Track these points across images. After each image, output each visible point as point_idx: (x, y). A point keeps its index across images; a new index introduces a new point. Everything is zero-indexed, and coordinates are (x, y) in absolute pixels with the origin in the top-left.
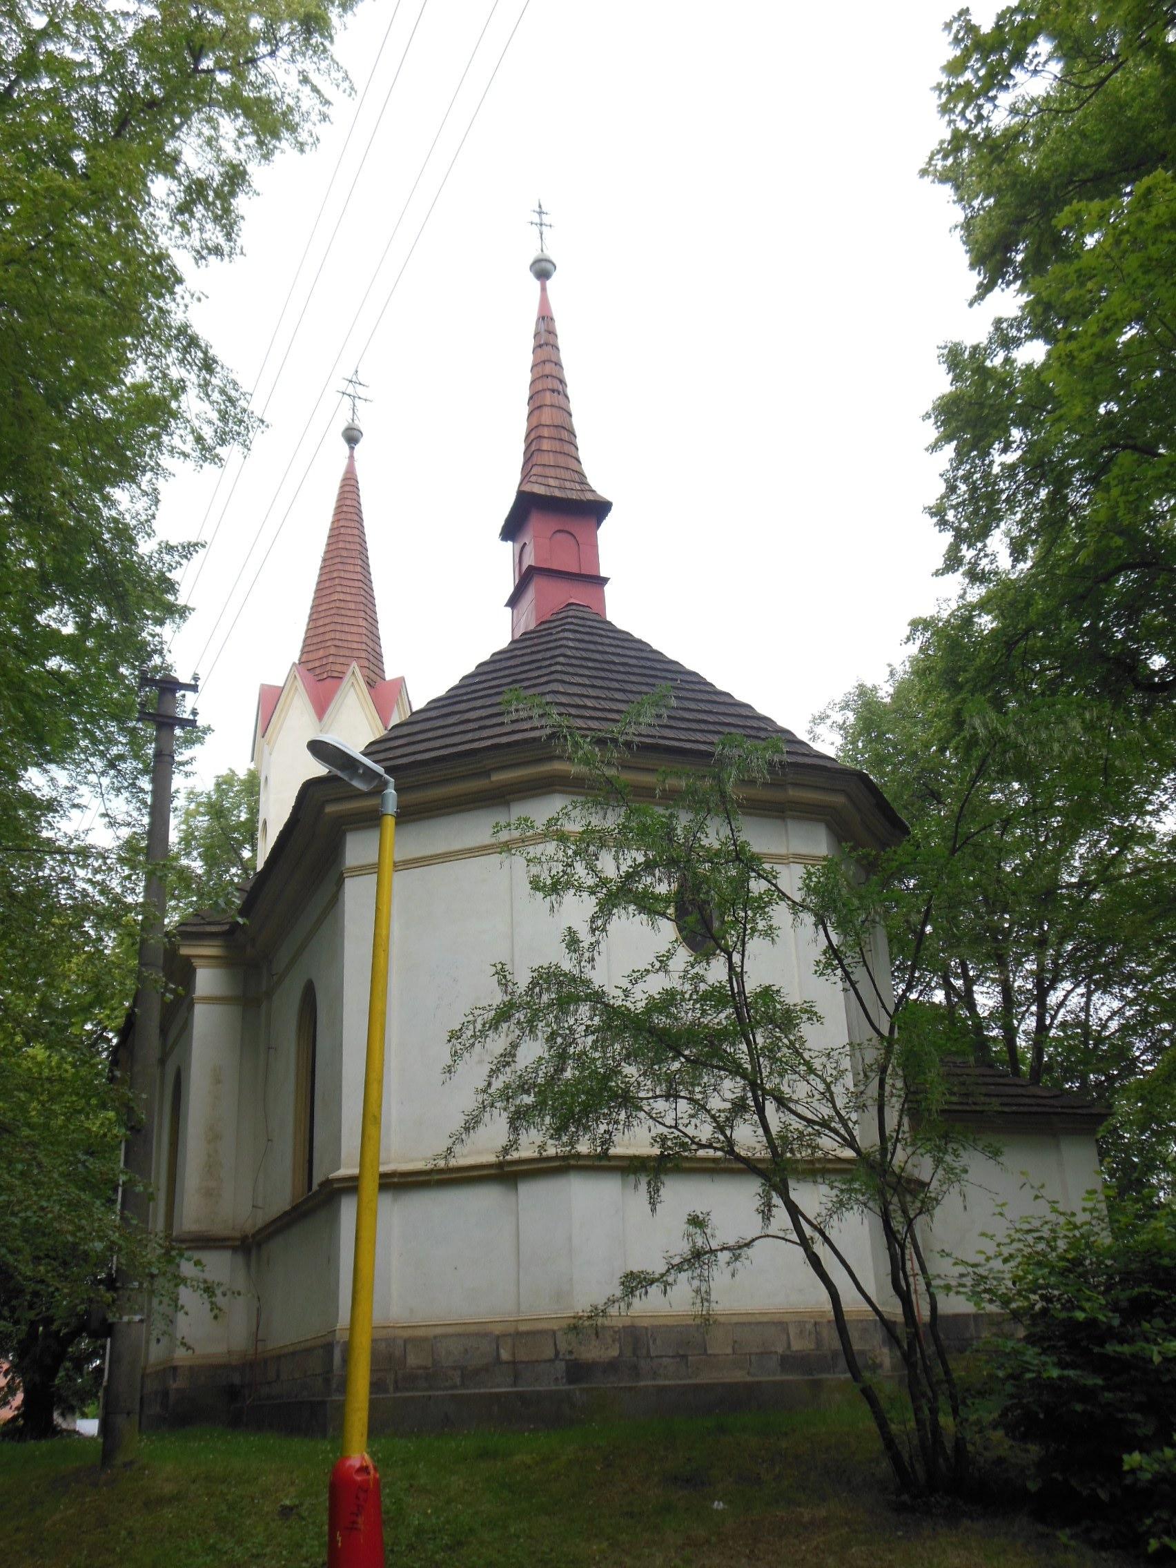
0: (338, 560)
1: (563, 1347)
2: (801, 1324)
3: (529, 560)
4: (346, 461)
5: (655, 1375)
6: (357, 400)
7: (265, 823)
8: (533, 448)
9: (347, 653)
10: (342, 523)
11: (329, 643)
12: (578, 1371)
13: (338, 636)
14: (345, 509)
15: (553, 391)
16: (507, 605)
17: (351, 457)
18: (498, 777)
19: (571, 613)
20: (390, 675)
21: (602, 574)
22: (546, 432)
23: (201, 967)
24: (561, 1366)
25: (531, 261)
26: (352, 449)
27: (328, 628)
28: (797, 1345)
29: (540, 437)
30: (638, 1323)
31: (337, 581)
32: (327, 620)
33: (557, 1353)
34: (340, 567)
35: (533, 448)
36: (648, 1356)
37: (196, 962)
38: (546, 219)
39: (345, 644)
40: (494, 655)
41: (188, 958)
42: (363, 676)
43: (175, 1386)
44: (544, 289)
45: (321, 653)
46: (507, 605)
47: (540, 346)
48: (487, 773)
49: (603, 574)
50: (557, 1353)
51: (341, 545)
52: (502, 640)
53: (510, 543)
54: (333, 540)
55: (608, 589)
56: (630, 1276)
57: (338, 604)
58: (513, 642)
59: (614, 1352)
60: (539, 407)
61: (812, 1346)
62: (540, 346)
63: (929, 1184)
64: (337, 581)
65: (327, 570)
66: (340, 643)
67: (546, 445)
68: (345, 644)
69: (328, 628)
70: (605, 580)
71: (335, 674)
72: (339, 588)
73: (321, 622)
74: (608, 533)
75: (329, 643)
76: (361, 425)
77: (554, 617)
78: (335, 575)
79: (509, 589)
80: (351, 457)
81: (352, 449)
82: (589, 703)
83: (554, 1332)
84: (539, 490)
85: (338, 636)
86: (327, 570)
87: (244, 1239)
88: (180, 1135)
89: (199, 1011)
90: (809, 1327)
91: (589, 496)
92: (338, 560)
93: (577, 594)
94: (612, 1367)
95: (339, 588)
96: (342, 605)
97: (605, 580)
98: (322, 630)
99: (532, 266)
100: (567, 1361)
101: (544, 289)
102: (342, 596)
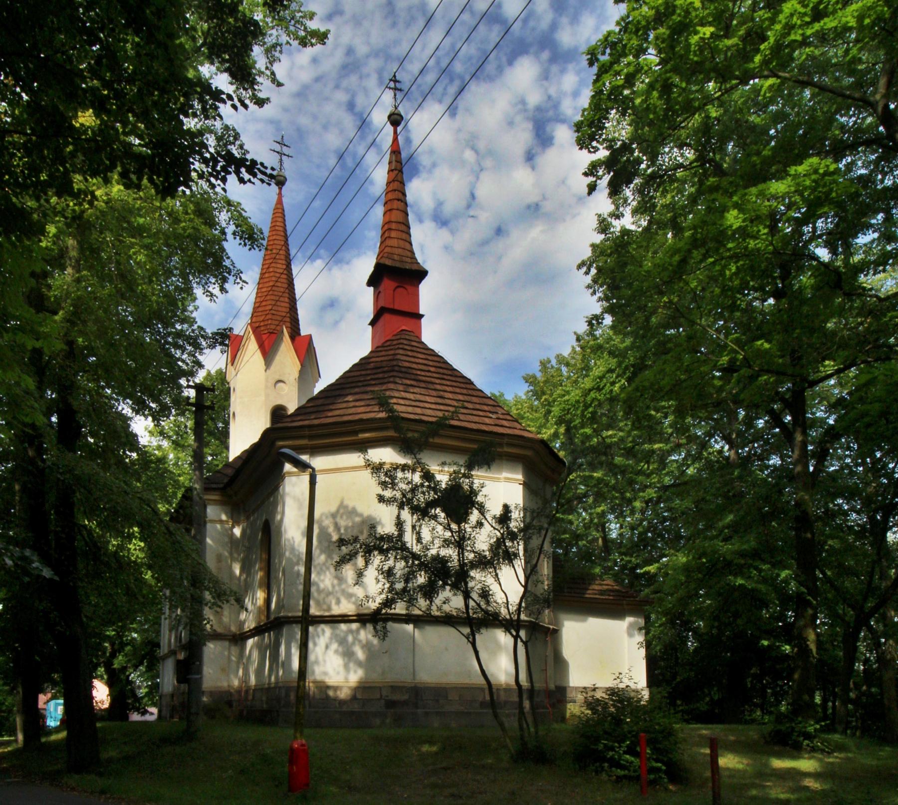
3: (382, 304)
4: (276, 197)
6: (284, 158)
7: (234, 414)
8: (386, 235)
15: (398, 200)
16: (370, 324)
17: (280, 194)
19: (403, 337)
22: (394, 226)
24: (383, 701)
25: (388, 114)
26: (280, 189)
30: (419, 685)
33: (381, 696)
35: (386, 235)
40: (361, 360)
46: (370, 324)
47: (392, 170)
48: (356, 433)
49: (421, 312)
52: (365, 349)
53: (372, 288)
55: (423, 320)
56: (380, 502)
58: (371, 352)
59: (405, 697)
60: (390, 210)
67: (393, 234)
70: (422, 316)
77: (394, 338)
79: (372, 317)
80: (280, 194)
81: (280, 189)
82: (432, 369)
84: (388, 262)
88: (438, 451)
91: (415, 267)
93: (405, 324)
94: (405, 703)
97: (422, 316)
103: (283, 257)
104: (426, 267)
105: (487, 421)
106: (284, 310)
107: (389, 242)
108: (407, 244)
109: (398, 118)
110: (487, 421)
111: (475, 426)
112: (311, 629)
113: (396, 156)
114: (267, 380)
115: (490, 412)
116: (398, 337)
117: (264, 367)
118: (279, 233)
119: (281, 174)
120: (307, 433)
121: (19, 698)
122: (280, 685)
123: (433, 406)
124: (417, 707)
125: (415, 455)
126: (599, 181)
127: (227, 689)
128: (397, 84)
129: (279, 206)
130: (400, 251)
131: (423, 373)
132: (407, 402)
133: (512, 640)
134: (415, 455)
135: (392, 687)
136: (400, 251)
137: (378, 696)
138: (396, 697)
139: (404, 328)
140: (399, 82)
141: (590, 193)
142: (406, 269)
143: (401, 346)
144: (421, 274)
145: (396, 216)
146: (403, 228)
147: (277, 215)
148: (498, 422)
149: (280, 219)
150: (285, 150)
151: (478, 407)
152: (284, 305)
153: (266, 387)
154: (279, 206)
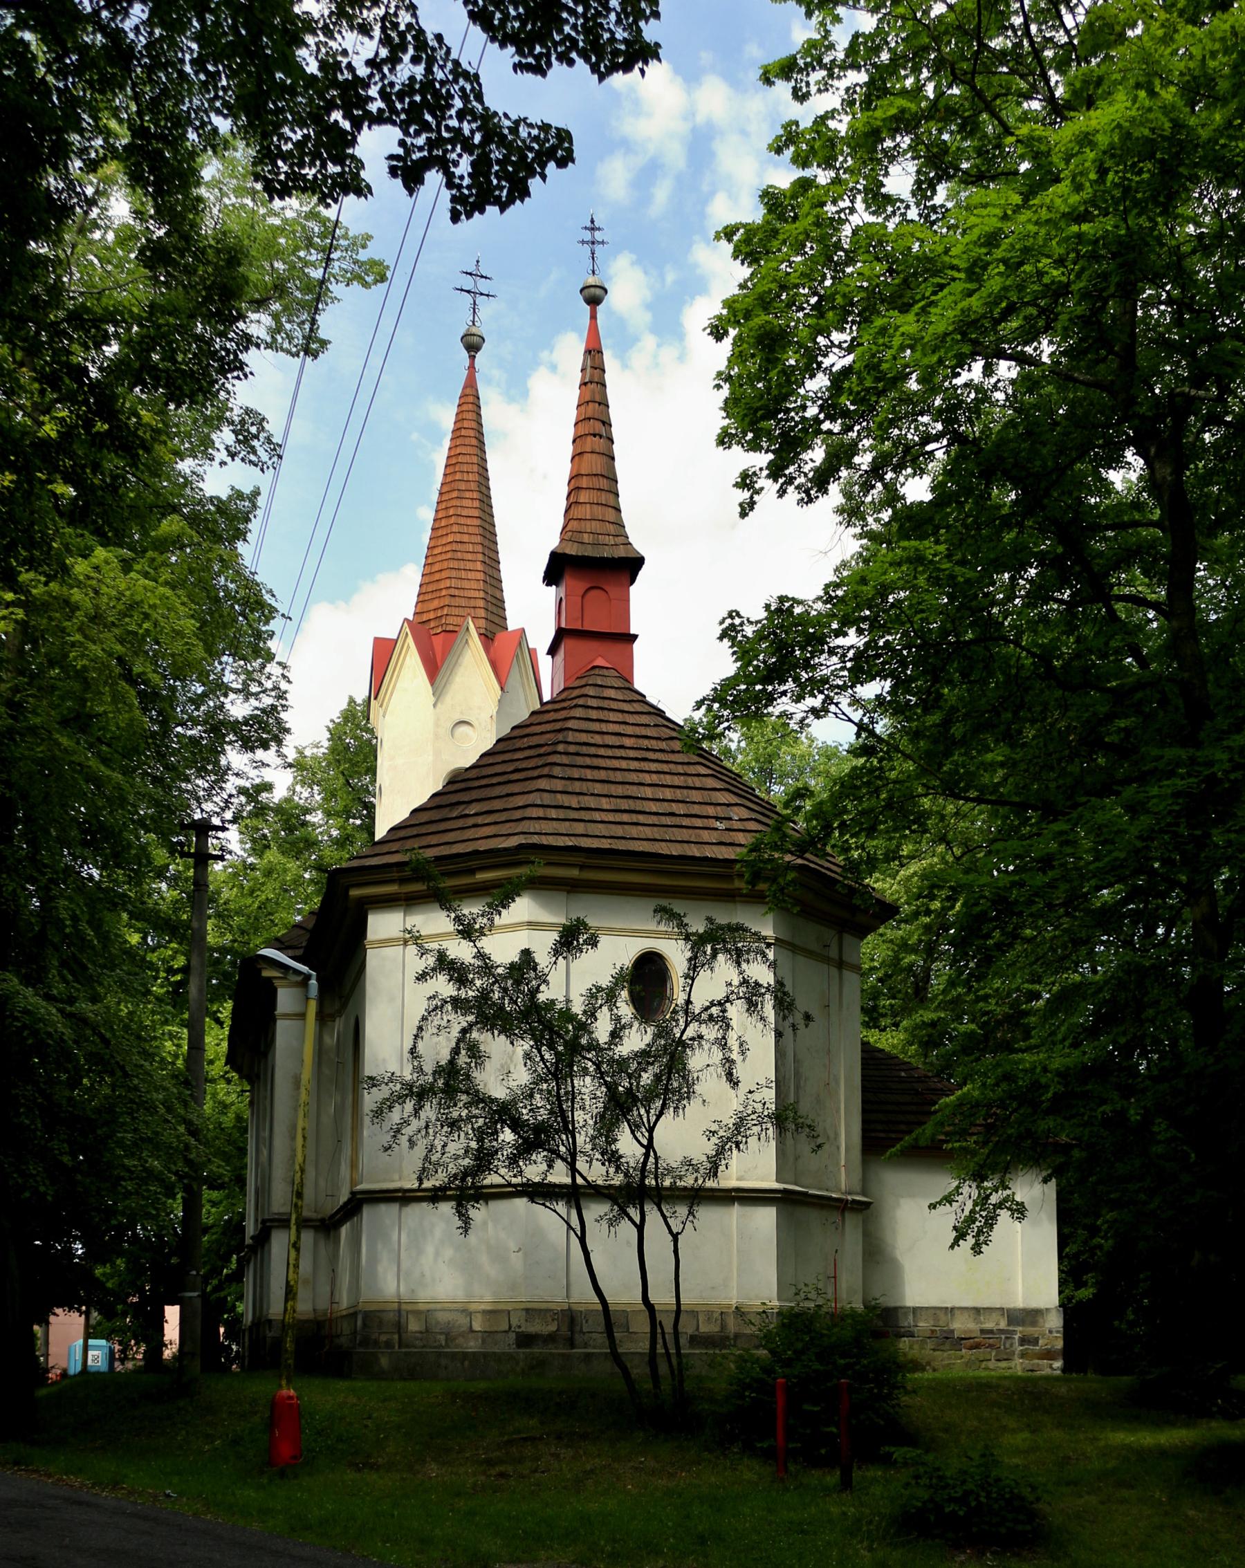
0: (455, 494)
1: (514, 1322)
2: (709, 1314)
5: (586, 1345)
6: (479, 299)
9: (463, 602)
10: (458, 450)
11: (444, 593)
12: (525, 1340)
13: (454, 583)
14: (463, 432)
15: (595, 435)
16: (548, 653)
17: (472, 367)
18: (482, 876)
20: (512, 625)
21: (632, 632)
22: (584, 482)
23: (282, 987)
24: (513, 1336)
26: (472, 358)
27: (444, 575)
28: (704, 1328)
29: (578, 488)
30: (575, 1307)
31: (453, 520)
32: (445, 565)
33: (510, 1327)
34: (457, 503)
36: (581, 1331)
37: (276, 983)
38: (598, 236)
39: (461, 593)
41: (270, 979)
42: (477, 628)
43: (270, 1335)
44: (593, 317)
45: (435, 604)
47: (585, 384)
48: (472, 872)
50: (510, 1327)
51: (458, 477)
54: (451, 470)
55: (637, 646)
57: (454, 547)
59: (553, 1328)
61: (717, 1329)
62: (585, 384)
63: (88, 1336)
64: (453, 520)
65: (443, 506)
66: (457, 592)
68: (461, 593)
69: (444, 575)
70: (635, 637)
71: (451, 628)
72: (455, 528)
73: (436, 567)
74: (640, 592)
75: (444, 593)
76: (482, 329)
78: (451, 512)
80: (472, 367)
81: (472, 358)
82: (628, 742)
83: (509, 1312)
84: (572, 550)
85: (454, 583)
86: (443, 506)
87: (322, 1220)
89: (280, 1025)
90: (716, 1315)
92: (455, 494)
93: (601, 656)
94: (551, 1338)
95: (455, 528)
96: (459, 547)
97: (635, 637)
98: (437, 577)
99: (581, 291)
100: (517, 1333)
101: (593, 317)
102: (458, 538)
103: (473, 486)
104: (643, 552)
105: (706, 836)
106: (474, 585)
107: (577, 512)
108: (611, 513)
109: (598, 292)
110: (706, 836)
111: (675, 850)
112: (454, 1203)
113: (593, 359)
114: (437, 724)
115: (717, 818)
116: (583, 682)
117: (433, 699)
118: (467, 441)
119: (474, 330)
120: (396, 875)
121: (1020, 1373)
122: (360, 1307)
123: (610, 817)
124: (572, 1346)
125: (474, 942)
126: (756, 498)
127: (311, 1316)
128: (597, 233)
129: (468, 391)
130: (595, 526)
131: (609, 752)
132: (561, 814)
133: (635, 1231)
134: (474, 942)
135: (527, 1310)
136: (595, 526)
137: (507, 1328)
138: (536, 1327)
139: (600, 662)
140: (599, 229)
141: (743, 514)
142: (603, 559)
143: (581, 701)
144: (633, 565)
145: (593, 463)
146: (604, 483)
147: (465, 407)
148: (727, 838)
149: (471, 416)
150: (483, 286)
151: (696, 809)
152: (473, 584)
153: (437, 736)
154: (468, 391)
